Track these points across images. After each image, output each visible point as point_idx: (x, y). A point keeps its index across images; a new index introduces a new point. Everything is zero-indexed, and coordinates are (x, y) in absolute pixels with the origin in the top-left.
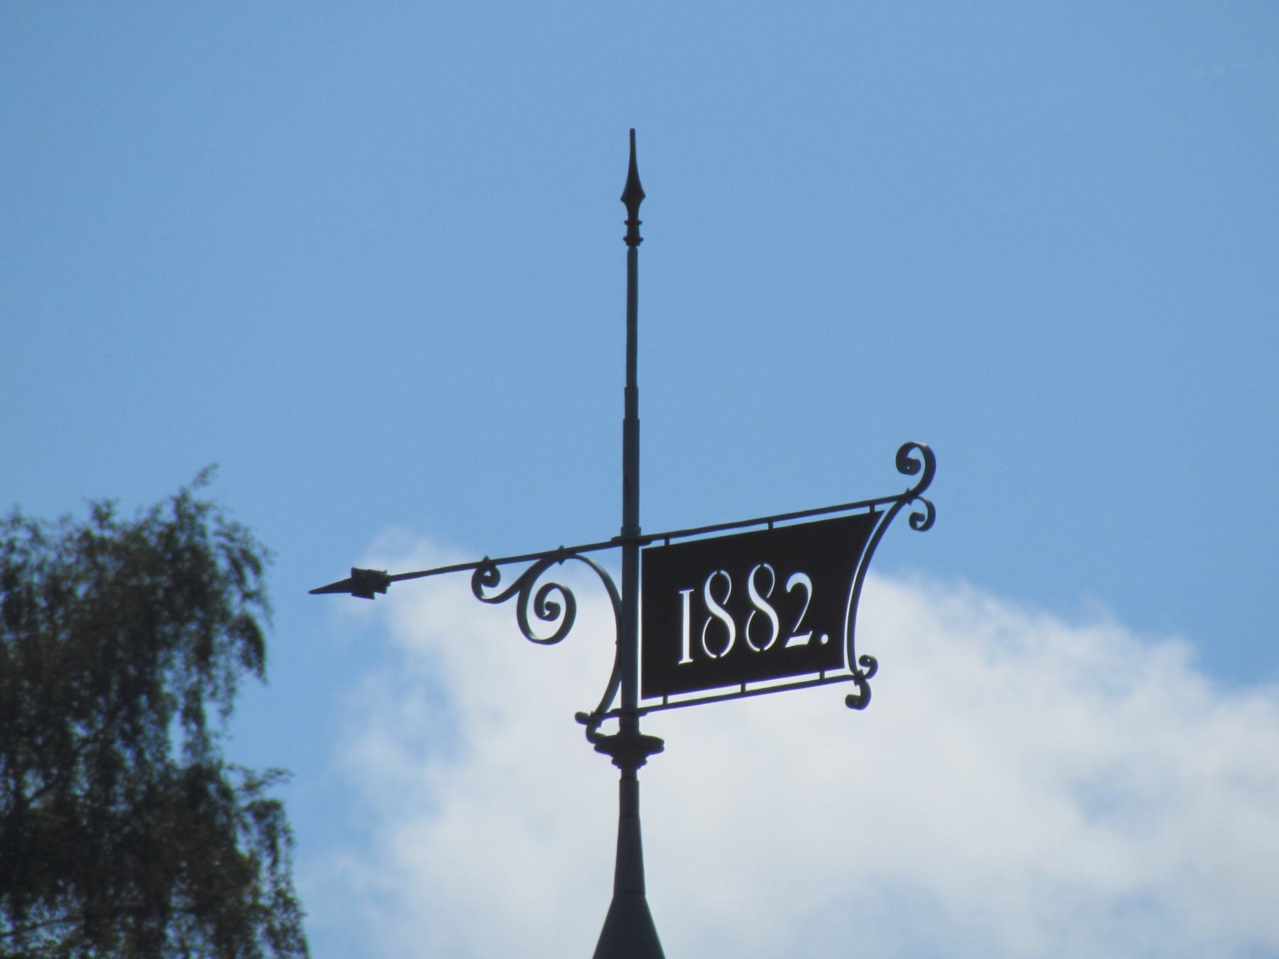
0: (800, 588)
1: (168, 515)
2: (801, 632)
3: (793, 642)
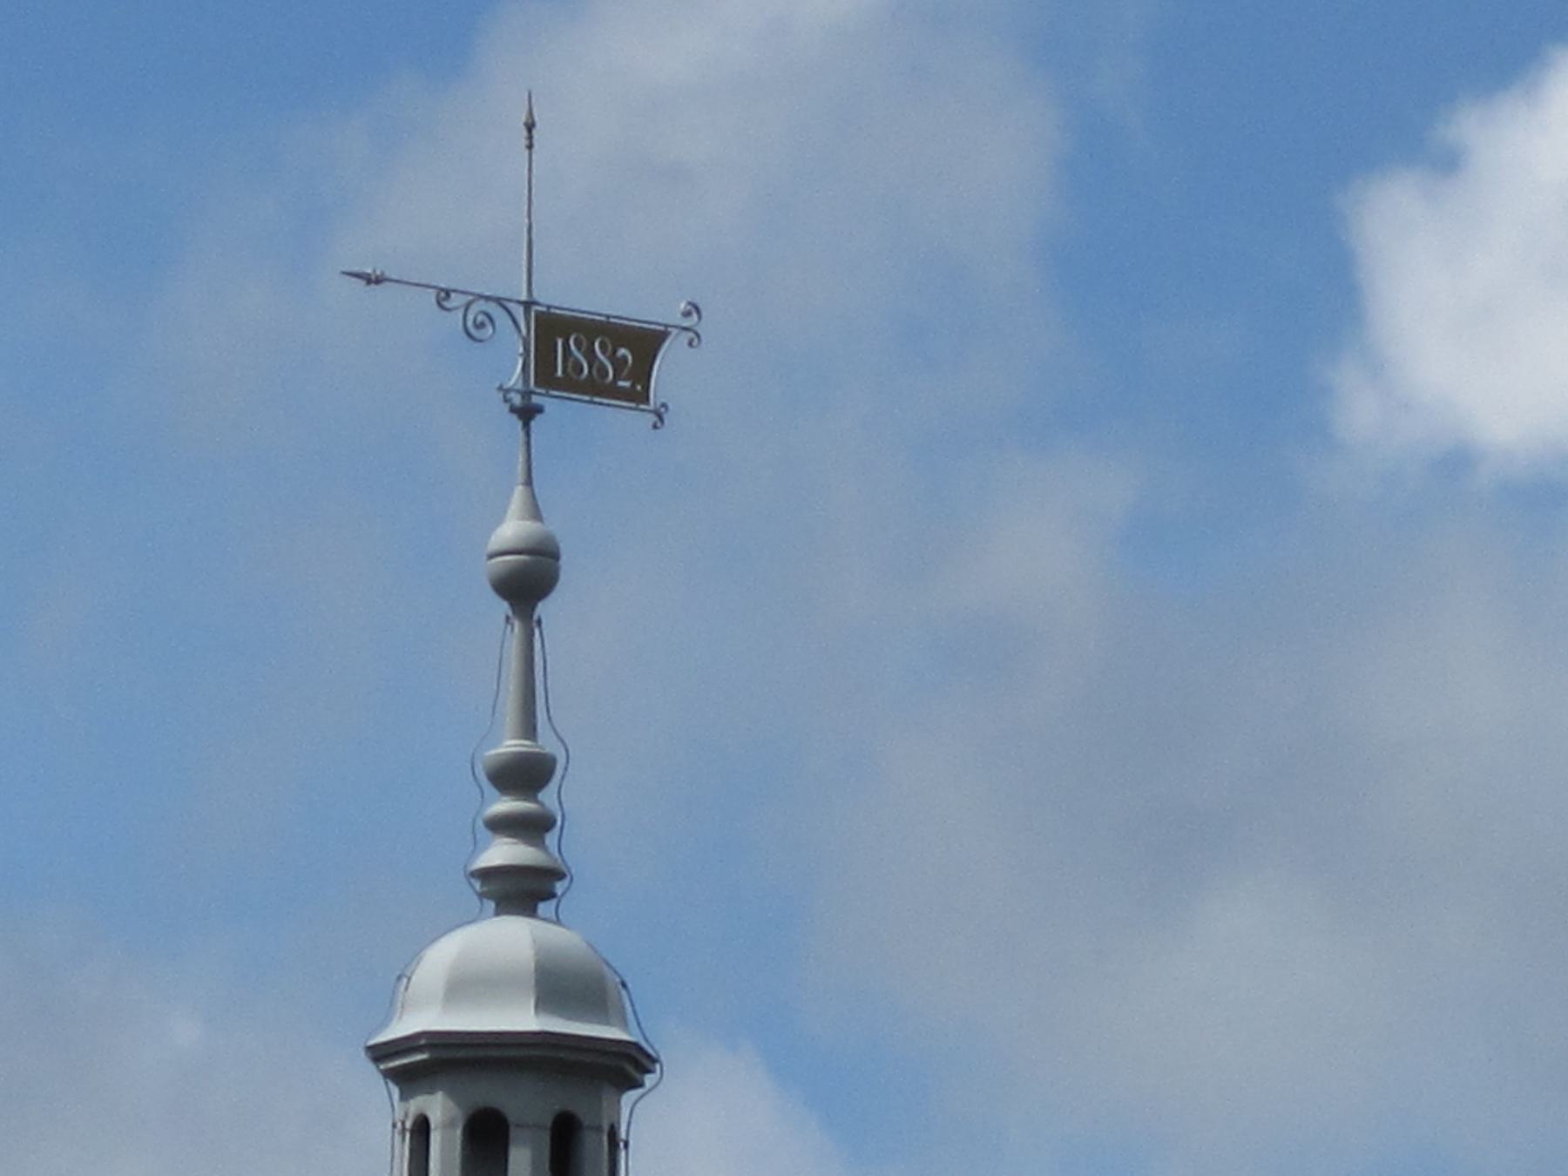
0: (624, 358)
1: (478, 885)
2: (625, 379)
3: (621, 383)
